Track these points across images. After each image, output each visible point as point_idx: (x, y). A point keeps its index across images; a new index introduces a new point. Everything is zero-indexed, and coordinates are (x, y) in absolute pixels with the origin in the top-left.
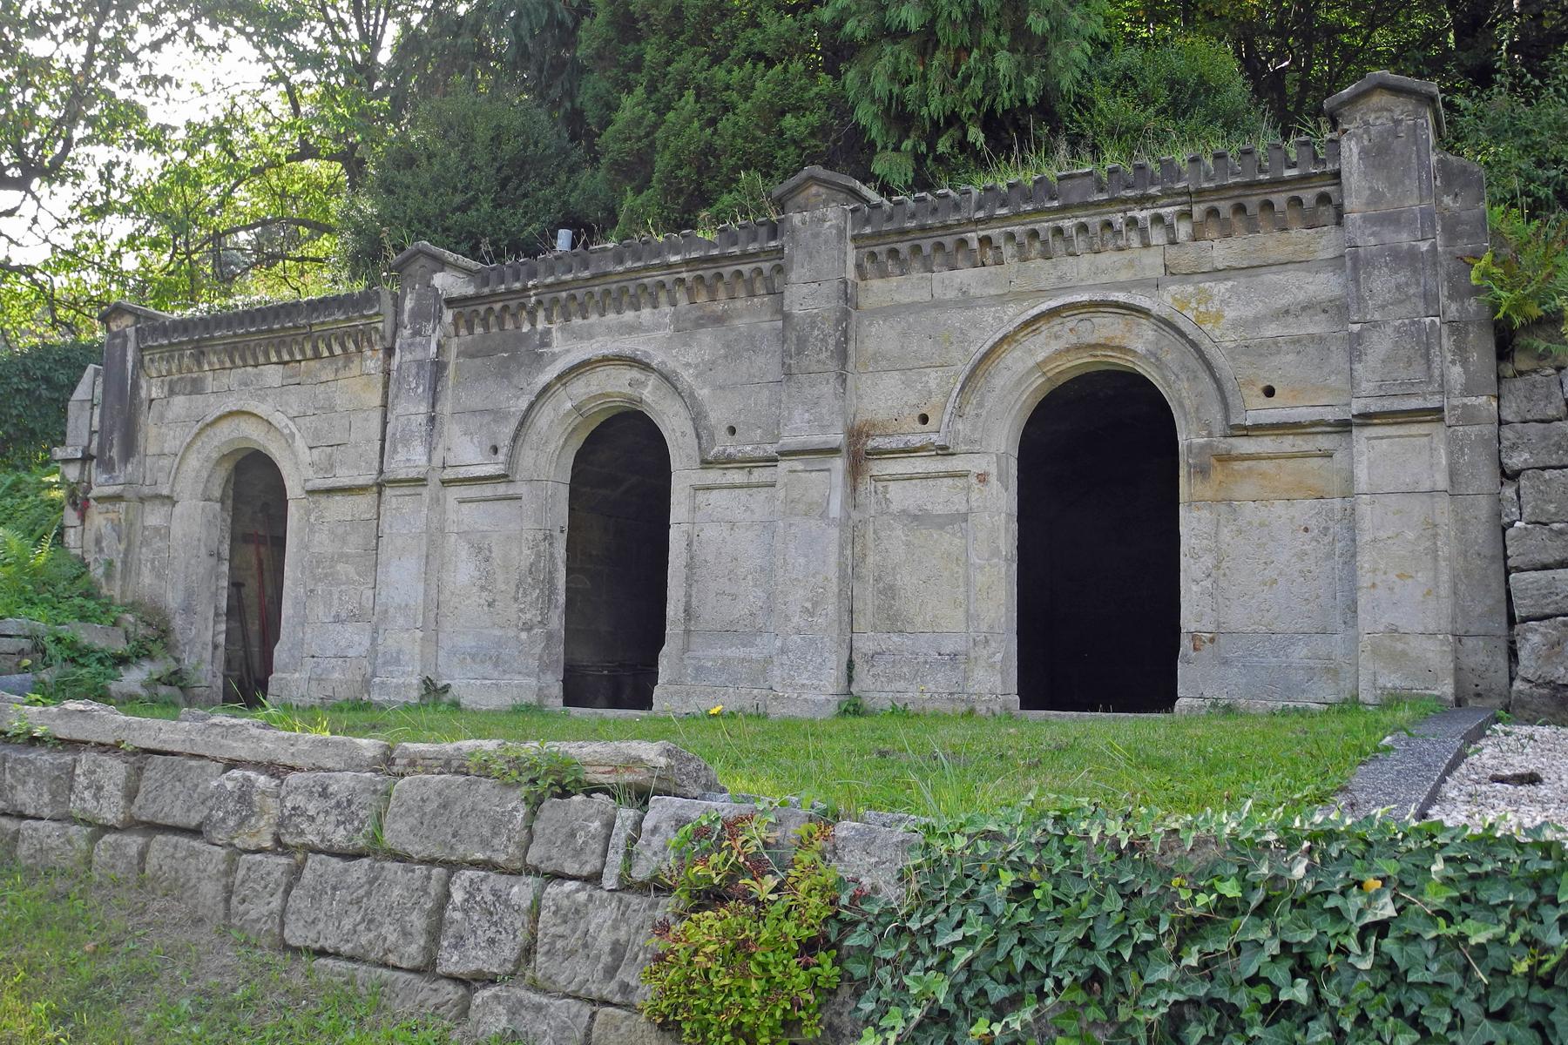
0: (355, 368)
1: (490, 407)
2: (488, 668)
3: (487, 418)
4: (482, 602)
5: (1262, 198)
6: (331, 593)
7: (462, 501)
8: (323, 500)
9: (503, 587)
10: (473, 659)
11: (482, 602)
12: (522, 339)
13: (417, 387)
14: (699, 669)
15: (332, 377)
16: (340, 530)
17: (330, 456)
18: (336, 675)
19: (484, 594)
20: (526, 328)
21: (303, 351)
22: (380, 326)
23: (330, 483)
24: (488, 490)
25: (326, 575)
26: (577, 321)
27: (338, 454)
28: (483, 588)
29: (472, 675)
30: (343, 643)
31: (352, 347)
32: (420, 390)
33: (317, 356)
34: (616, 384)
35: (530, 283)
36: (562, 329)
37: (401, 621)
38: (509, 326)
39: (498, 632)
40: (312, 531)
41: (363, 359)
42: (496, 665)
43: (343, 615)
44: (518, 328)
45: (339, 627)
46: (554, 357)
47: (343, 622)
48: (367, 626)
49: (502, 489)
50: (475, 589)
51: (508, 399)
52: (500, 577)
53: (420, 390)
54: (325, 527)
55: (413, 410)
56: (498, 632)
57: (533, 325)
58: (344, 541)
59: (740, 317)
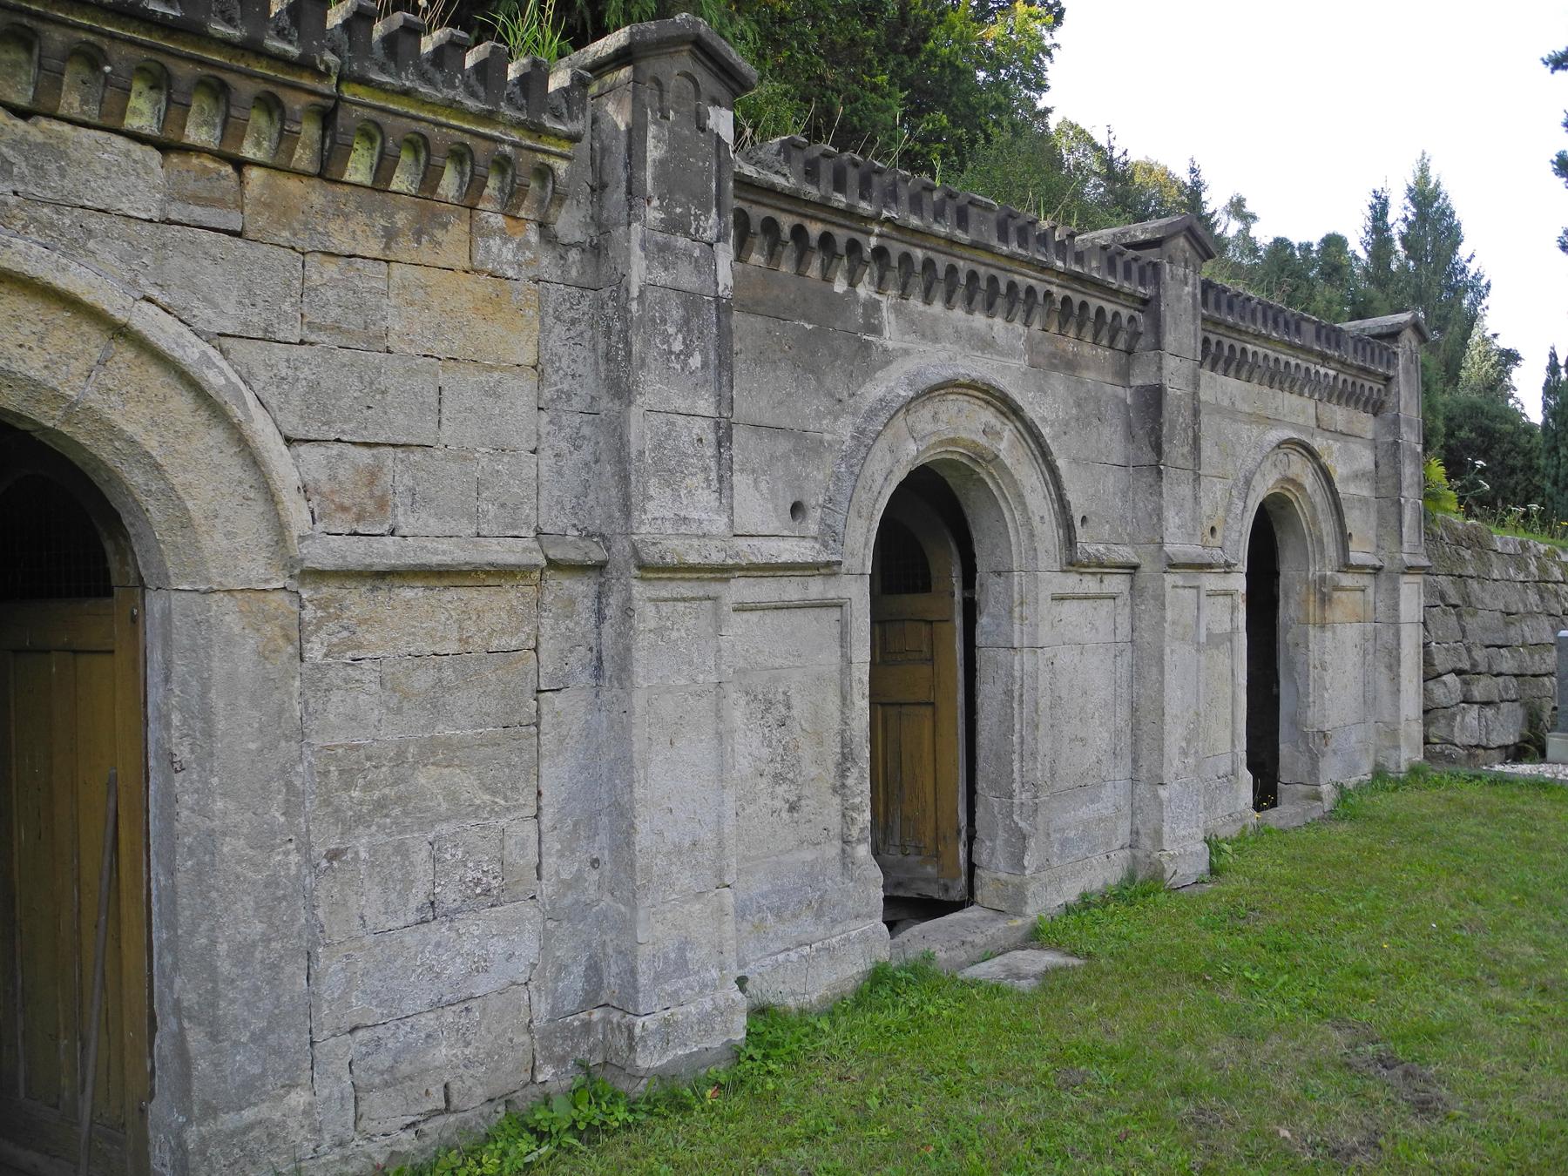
0: (452, 239)
1: (786, 422)
2: (806, 925)
3: (783, 445)
4: (779, 804)
5: (769, 212)
6: (402, 850)
7: (741, 608)
8: (357, 600)
9: (813, 771)
10: (779, 916)
11: (779, 804)
12: (836, 306)
13: (687, 353)
14: (1064, 843)
15: (374, 248)
16: (422, 680)
17: (373, 476)
18: (442, 1052)
19: (781, 790)
20: (840, 286)
21: (286, 139)
22: (561, 167)
23: (387, 553)
24: (791, 590)
25: (381, 805)
26: (915, 303)
27: (397, 473)
28: (778, 778)
29: (779, 945)
30: (456, 968)
31: (449, 184)
32: (696, 361)
33: (327, 171)
34: (969, 423)
35: (885, 213)
36: (897, 310)
37: (685, 880)
38: (814, 271)
39: (808, 855)
40: (316, 682)
41: (476, 231)
42: (819, 915)
43: (450, 897)
44: (827, 278)
45: (439, 931)
46: (888, 358)
47: (450, 915)
48: (528, 910)
49: (816, 588)
50: (763, 784)
51: (819, 416)
52: (807, 752)
53: (696, 361)
54: (368, 673)
55: (683, 405)
56: (808, 855)
57: (852, 284)
58: (435, 706)
59: (1088, 368)
